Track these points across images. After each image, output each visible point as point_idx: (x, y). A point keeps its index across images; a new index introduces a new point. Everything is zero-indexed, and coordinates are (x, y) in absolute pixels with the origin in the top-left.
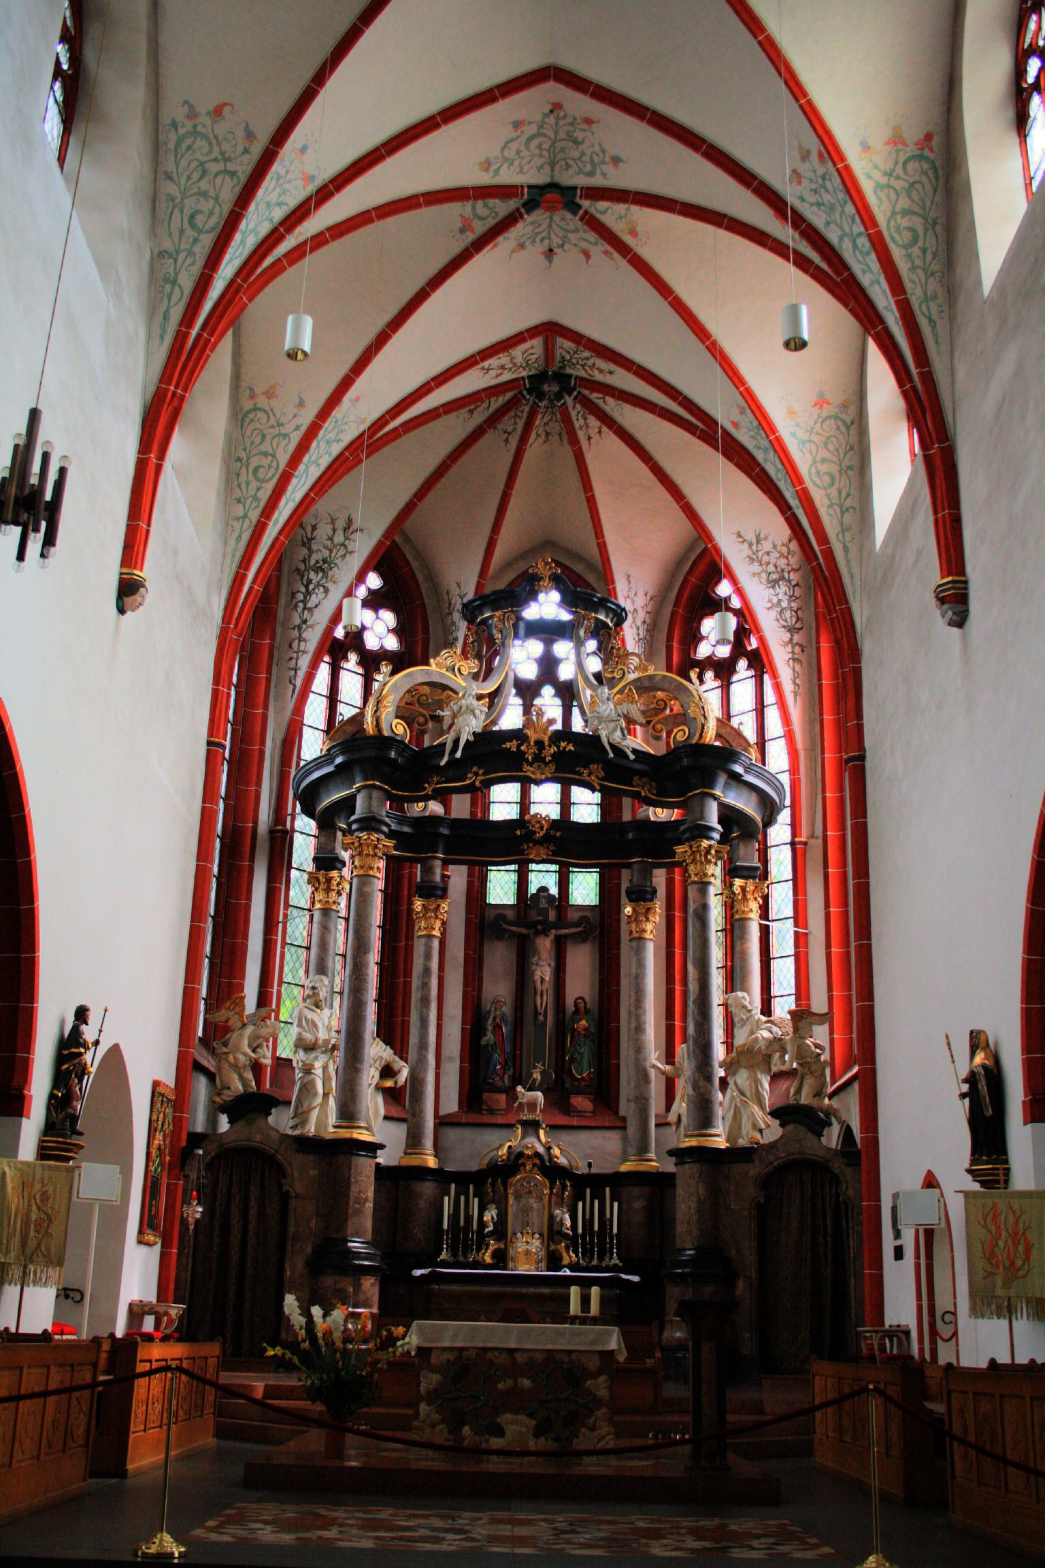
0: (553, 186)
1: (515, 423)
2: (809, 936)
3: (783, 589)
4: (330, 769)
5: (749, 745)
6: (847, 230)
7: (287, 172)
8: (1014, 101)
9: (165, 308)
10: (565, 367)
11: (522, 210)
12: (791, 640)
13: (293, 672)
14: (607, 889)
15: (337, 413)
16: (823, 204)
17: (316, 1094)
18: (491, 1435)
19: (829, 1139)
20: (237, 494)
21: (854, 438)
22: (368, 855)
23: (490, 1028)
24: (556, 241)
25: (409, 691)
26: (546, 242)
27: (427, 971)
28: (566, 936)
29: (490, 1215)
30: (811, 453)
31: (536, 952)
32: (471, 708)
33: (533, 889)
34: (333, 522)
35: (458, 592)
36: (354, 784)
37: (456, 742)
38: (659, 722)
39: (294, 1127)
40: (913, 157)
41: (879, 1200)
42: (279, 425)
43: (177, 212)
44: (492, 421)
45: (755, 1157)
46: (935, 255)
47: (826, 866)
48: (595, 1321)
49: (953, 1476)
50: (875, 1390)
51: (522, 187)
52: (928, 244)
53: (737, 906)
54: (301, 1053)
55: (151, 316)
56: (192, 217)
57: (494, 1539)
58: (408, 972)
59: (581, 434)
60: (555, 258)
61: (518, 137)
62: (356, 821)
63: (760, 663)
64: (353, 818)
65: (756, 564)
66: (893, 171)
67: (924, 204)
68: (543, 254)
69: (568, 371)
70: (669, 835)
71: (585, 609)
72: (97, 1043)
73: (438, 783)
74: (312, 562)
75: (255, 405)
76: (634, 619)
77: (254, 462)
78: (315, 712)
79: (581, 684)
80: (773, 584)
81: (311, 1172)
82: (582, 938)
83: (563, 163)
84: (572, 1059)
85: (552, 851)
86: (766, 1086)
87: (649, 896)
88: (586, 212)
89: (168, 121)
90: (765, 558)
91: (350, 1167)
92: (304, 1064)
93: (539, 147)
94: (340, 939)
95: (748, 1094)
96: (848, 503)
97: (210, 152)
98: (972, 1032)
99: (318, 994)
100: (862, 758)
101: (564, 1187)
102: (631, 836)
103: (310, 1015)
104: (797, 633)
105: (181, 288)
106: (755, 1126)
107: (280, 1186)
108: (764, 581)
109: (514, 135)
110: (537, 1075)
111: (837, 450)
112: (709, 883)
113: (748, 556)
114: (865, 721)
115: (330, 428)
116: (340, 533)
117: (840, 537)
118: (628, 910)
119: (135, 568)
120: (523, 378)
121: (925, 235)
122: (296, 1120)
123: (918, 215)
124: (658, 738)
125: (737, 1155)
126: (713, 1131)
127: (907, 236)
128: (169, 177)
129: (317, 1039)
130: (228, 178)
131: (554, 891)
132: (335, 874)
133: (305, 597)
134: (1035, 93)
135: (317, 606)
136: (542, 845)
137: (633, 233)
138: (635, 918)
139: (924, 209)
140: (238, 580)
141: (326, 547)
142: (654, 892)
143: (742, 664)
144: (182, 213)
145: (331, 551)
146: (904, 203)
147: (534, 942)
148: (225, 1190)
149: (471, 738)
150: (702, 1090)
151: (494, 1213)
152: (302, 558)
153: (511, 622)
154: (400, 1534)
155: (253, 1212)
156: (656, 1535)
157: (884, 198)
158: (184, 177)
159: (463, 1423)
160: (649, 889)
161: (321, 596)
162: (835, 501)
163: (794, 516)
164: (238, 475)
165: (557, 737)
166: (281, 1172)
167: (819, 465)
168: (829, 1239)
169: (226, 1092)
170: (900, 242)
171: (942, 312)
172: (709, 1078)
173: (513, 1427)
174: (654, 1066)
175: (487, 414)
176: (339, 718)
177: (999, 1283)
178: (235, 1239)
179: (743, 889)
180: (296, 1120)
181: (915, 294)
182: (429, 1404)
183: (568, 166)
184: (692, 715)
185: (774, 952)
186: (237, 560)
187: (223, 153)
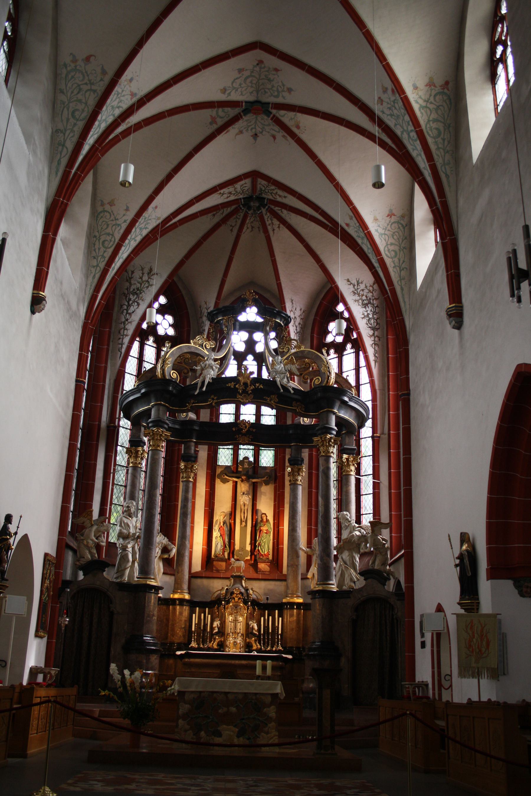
1: (236, 221)
2: (380, 484)
3: (370, 308)
4: (138, 395)
6: (405, 128)
7: (123, 91)
11: (242, 114)
12: (374, 334)
13: (120, 346)
15: (145, 214)
16: (393, 115)
17: (128, 561)
19: (389, 586)
20: (94, 254)
22: (157, 439)
26: (254, 130)
28: (257, 482)
29: (216, 624)
30: (385, 240)
32: (211, 365)
33: (241, 458)
34: (142, 269)
35: (205, 306)
38: (306, 374)
39: (117, 578)
43: (65, 109)
44: (224, 220)
46: (449, 142)
47: (389, 448)
48: (269, 678)
51: (242, 102)
53: (344, 468)
56: (73, 112)
59: (269, 228)
64: (150, 420)
65: (357, 295)
66: (429, 99)
68: (252, 136)
73: (193, 403)
74: (131, 290)
76: (295, 322)
77: (103, 238)
80: (365, 306)
84: (259, 545)
86: (358, 560)
90: (361, 292)
92: (123, 546)
93: (251, 82)
95: (348, 563)
96: (403, 266)
97: (83, 80)
98: (461, 533)
99: (130, 510)
100: (409, 394)
101: (254, 609)
102: (291, 432)
103: (126, 520)
104: (377, 331)
106: (352, 580)
108: (360, 304)
109: (239, 76)
111: (398, 239)
113: (353, 292)
115: (142, 222)
117: (399, 282)
120: (240, 199)
122: (119, 574)
123: (440, 122)
125: (342, 594)
127: (435, 132)
128: (62, 92)
129: (129, 533)
130: (92, 93)
131: (252, 459)
132: (140, 449)
133: (127, 308)
135: (133, 312)
136: (246, 436)
137: (298, 127)
138: (292, 474)
141: (139, 283)
143: (349, 346)
145: (141, 284)
146: (434, 116)
149: (211, 381)
152: (126, 288)
157: (424, 113)
160: (300, 459)
161: (136, 307)
164: (94, 244)
167: (389, 246)
169: (82, 559)
171: (452, 171)
173: (227, 732)
175: (222, 217)
176: (143, 370)
179: (347, 459)
180: (119, 574)
181: (439, 162)
183: (266, 92)
186: (93, 288)
187: (90, 81)
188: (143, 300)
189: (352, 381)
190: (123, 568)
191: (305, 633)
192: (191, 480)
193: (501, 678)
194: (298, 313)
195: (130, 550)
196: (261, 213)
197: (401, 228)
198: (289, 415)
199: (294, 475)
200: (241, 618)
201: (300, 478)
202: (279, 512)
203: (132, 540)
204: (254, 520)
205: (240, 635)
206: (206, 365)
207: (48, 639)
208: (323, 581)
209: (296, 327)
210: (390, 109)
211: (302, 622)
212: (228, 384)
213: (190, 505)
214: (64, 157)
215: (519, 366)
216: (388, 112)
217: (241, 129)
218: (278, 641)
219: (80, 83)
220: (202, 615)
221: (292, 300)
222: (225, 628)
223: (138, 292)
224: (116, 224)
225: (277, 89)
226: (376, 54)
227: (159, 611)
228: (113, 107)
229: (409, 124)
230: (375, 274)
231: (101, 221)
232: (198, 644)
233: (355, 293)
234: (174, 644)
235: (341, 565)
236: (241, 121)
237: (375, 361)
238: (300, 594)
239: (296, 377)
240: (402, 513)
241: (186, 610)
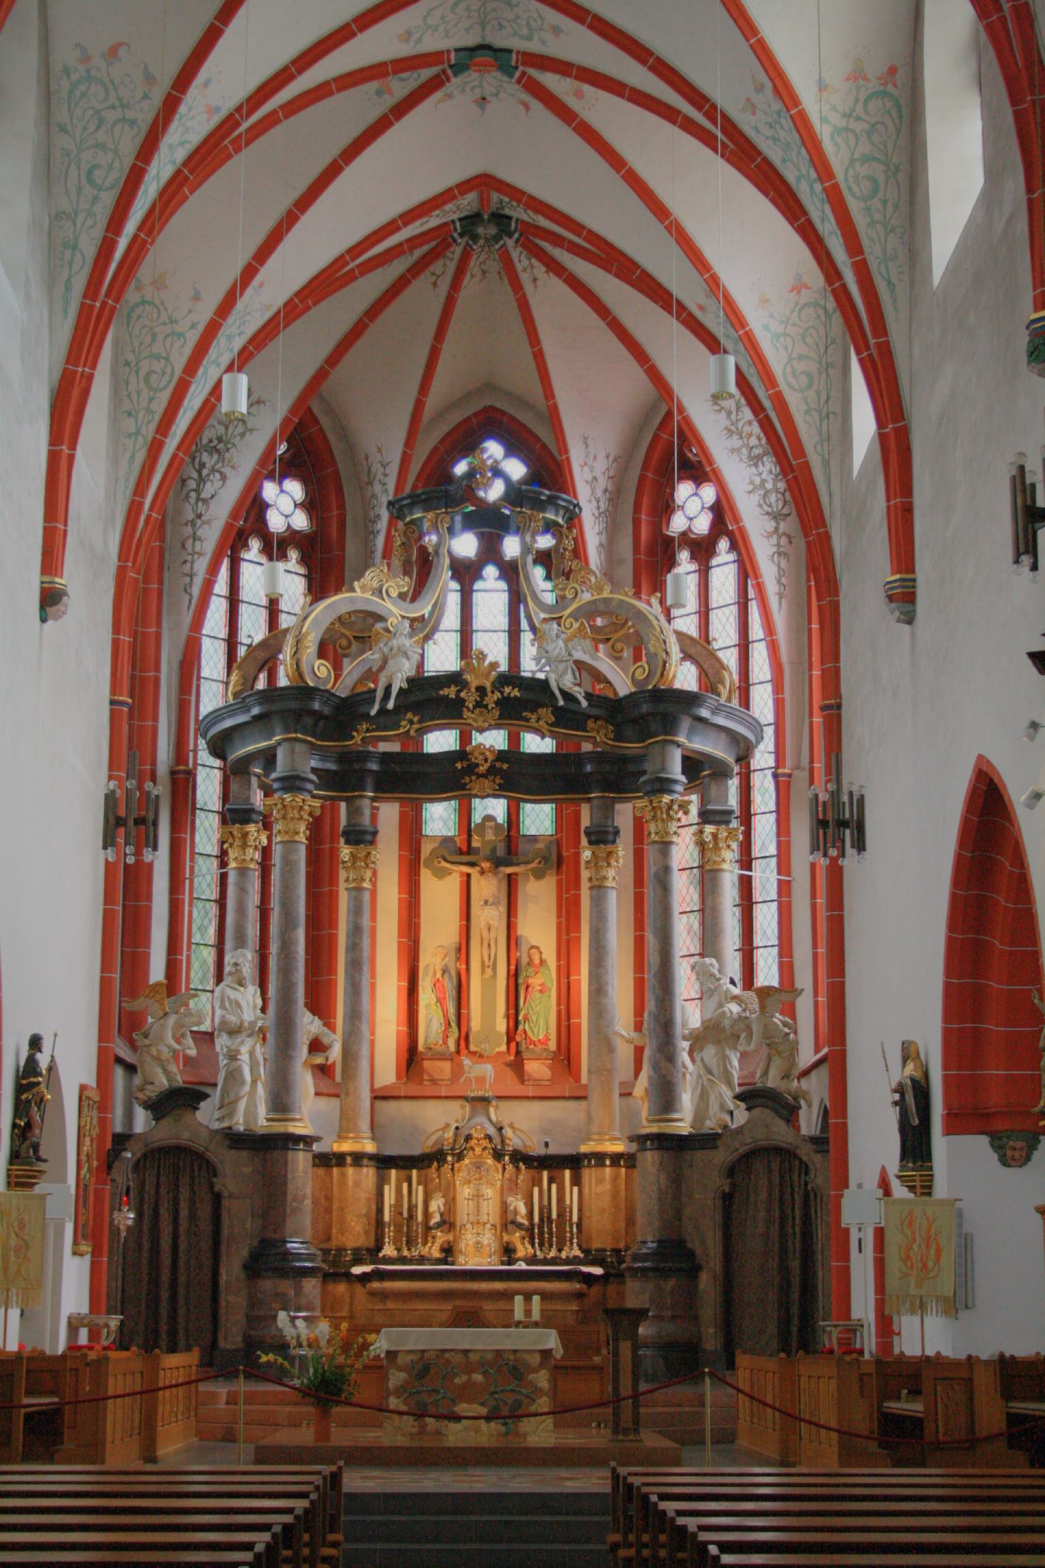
10: (503, 208)
12: (777, 529)
14: (566, 823)
17: (243, 1082)
20: (127, 405)
26: (478, 91)
28: (516, 874)
29: (436, 1205)
30: (786, 349)
35: (379, 458)
36: (274, 735)
37: (388, 689)
38: (619, 640)
39: (221, 1119)
40: (875, 95)
42: (171, 322)
43: (73, 166)
44: (416, 270)
45: (719, 1143)
46: (896, 207)
48: (536, 1325)
51: (448, 52)
56: (90, 173)
59: (525, 278)
60: (488, 106)
62: (275, 780)
63: (740, 545)
64: (274, 776)
65: (735, 437)
71: (532, 509)
73: (368, 731)
74: (205, 441)
77: (145, 367)
84: (526, 1019)
85: (499, 785)
86: (736, 1063)
90: (747, 429)
91: (286, 1164)
92: (229, 1050)
95: (715, 1072)
97: (106, 99)
99: (240, 971)
100: (839, 706)
101: (517, 1168)
102: (589, 768)
103: (233, 994)
104: (784, 520)
105: (82, 254)
106: (722, 1107)
107: (212, 1185)
108: (744, 457)
111: (817, 344)
112: (671, 843)
113: (726, 428)
114: (842, 664)
117: (819, 449)
118: (586, 854)
119: (56, 575)
120: (453, 222)
121: (886, 184)
122: (223, 1112)
125: (702, 1141)
126: (675, 1116)
128: (63, 129)
129: (242, 1022)
130: (127, 128)
133: (198, 485)
135: (213, 497)
138: (594, 863)
140: (134, 510)
142: (617, 833)
143: (723, 544)
145: (227, 428)
146: (864, 148)
148: (152, 1192)
149: (405, 686)
150: (663, 1071)
153: (446, 525)
155: (184, 1212)
160: (611, 829)
161: (218, 484)
162: (812, 405)
164: (127, 383)
165: (505, 680)
166: (212, 1171)
167: (795, 363)
168: (797, 1229)
169: (150, 1087)
170: (859, 194)
177: (913, 1281)
179: (715, 836)
180: (223, 1112)
181: (873, 254)
183: (501, 27)
186: (132, 485)
187: (120, 99)
188: (233, 467)
190: (232, 1098)
191: (630, 1222)
192: (366, 885)
193: (961, 1314)
194: (601, 466)
197: (823, 317)
199: (597, 868)
200: (489, 1191)
201: (611, 873)
202: (568, 941)
203: (250, 1036)
204: (513, 962)
205: (488, 1226)
206: (391, 650)
207: (93, 1256)
208: (660, 1114)
209: (598, 501)
211: (623, 1194)
212: (442, 688)
213: (366, 941)
218: (571, 1238)
220: (405, 1186)
221: (586, 439)
222: (455, 1213)
224: (173, 333)
225: (528, 23)
230: (766, 425)
232: (398, 1250)
233: (730, 432)
234: (346, 1250)
237: (781, 596)
238: (617, 1134)
241: (368, 1174)
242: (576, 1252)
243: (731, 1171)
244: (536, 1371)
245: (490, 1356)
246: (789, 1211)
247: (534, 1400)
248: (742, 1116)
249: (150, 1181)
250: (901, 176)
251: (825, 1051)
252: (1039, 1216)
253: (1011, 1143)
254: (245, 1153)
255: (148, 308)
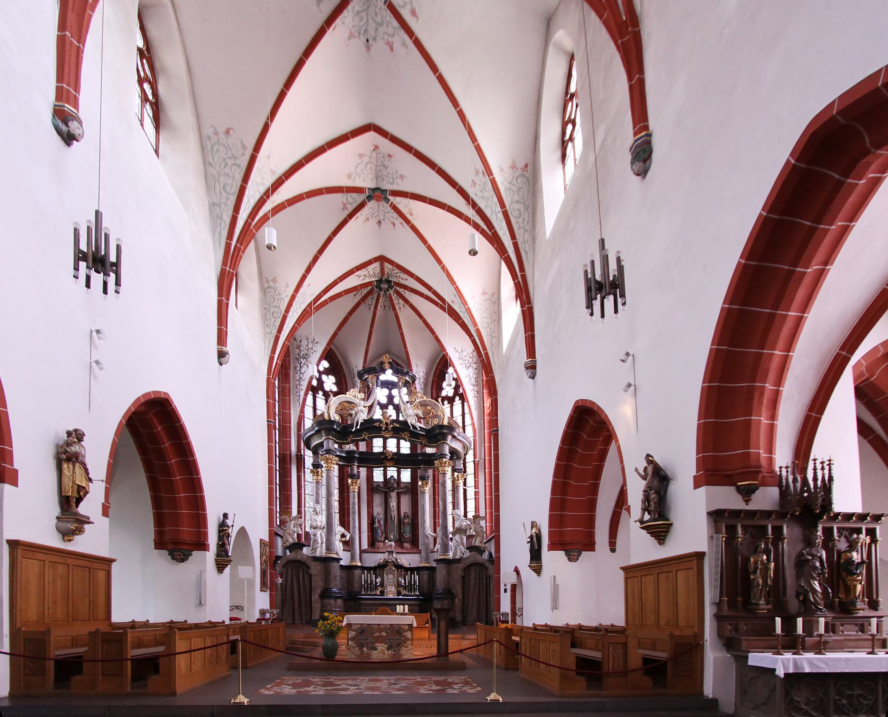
0: (378, 189)
1: (372, 301)
2: (480, 492)
4: (314, 432)
5: (459, 426)
6: (494, 209)
7: (263, 168)
8: (561, 147)
9: (219, 230)
11: (366, 200)
12: (474, 389)
13: (298, 397)
16: (484, 197)
17: (318, 543)
18: (373, 650)
19: (485, 557)
21: (496, 309)
22: (329, 463)
23: (376, 522)
24: (381, 217)
25: (339, 404)
26: (377, 218)
27: (354, 503)
28: (400, 492)
29: (379, 580)
30: (480, 314)
31: (391, 497)
33: (388, 477)
34: (307, 339)
36: (323, 437)
41: (500, 574)
44: (364, 299)
45: (461, 562)
46: (528, 222)
48: (406, 614)
49: (521, 662)
50: (496, 641)
52: (525, 217)
53: (456, 482)
54: (312, 529)
55: (214, 232)
56: (224, 187)
57: (368, 689)
58: (348, 504)
59: (397, 306)
61: (362, 162)
62: (324, 451)
63: (463, 398)
64: (323, 450)
66: (512, 181)
67: (524, 197)
68: (377, 223)
69: (390, 279)
70: (433, 458)
72: (233, 526)
74: (301, 355)
75: (269, 285)
76: (419, 381)
77: (272, 310)
78: (309, 413)
79: (401, 404)
81: (319, 568)
82: (405, 493)
83: (381, 178)
86: (465, 540)
87: (427, 479)
88: (392, 203)
89: (206, 135)
93: (371, 168)
94: (323, 492)
96: (493, 335)
100: (498, 430)
101: (402, 571)
102: (420, 458)
103: (314, 517)
105: (224, 221)
107: (308, 572)
108: (464, 367)
109: (359, 161)
110: (392, 537)
112: (446, 473)
116: (310, 343)
118: (420, 483)
120: (373, 281)
123: (521, 203)
124: (428, 424)
127: (517, 213)
128: (211, 165)
130: (237, 168)
131: (396, 477)
132: (319, 470)
134: (570, 142)
137: (411, 214)
139: (524, 200)
140: (271, 359)
141: (306, 350)
143: (457, 398)
144: (219, 184)
145: (308, 351)
146: (516, 197)
147: (390, 494)
149: (363, 421)
151: (380, 579)
154: (335, 687)
156: (422, 684)
157: (509, 195)
158: (218, 166)
159: (363, 647)
163: (474, 339)
164: (266, 315)
165: (393, 421)
166: (308, 567)
169: (287, 542)
171: (530, 248)
172: (447, 537)
173: (380, 647)
174: (429, 534)
175: (361, 296)
178: (295, 589)
179: (458, 476)
180: (313, 551)
182: (352, 641)
184: (439, 414)
185: (468, 497)
188: (310, 363)
189: (460, 422)
195: (319, 536)
196: (390, 293)
197: (492, 304)
198: (419, 446)
199: (423, 487)
207: (270, 592)
210: (481, 191)
214: (223, 229)
215: (577, 402)
216: (480, 194)
217: (368, 216)
219: (225, 157)
223: (306, 357)
226: (468, 133)
227: (340, 573)
228: (257, 184)
229: (496, 206)
230: (474, 342)
231: (268, 295)
235: (454, 544)
236: (366, 207)
239: (422, 420)
240: (493, 510)
242: (418, 593)
243: (465, 570)
244: (407, 631)
245: (388, 626)
246: (481, 581)
247: (406, 643)
248: (467, 554)
249: (290, 571)
250: (529, 210)
251: (494, 534)
252: (622, 571)
253: (573, 554)
254: (318, 563)
255: (271, 289)
